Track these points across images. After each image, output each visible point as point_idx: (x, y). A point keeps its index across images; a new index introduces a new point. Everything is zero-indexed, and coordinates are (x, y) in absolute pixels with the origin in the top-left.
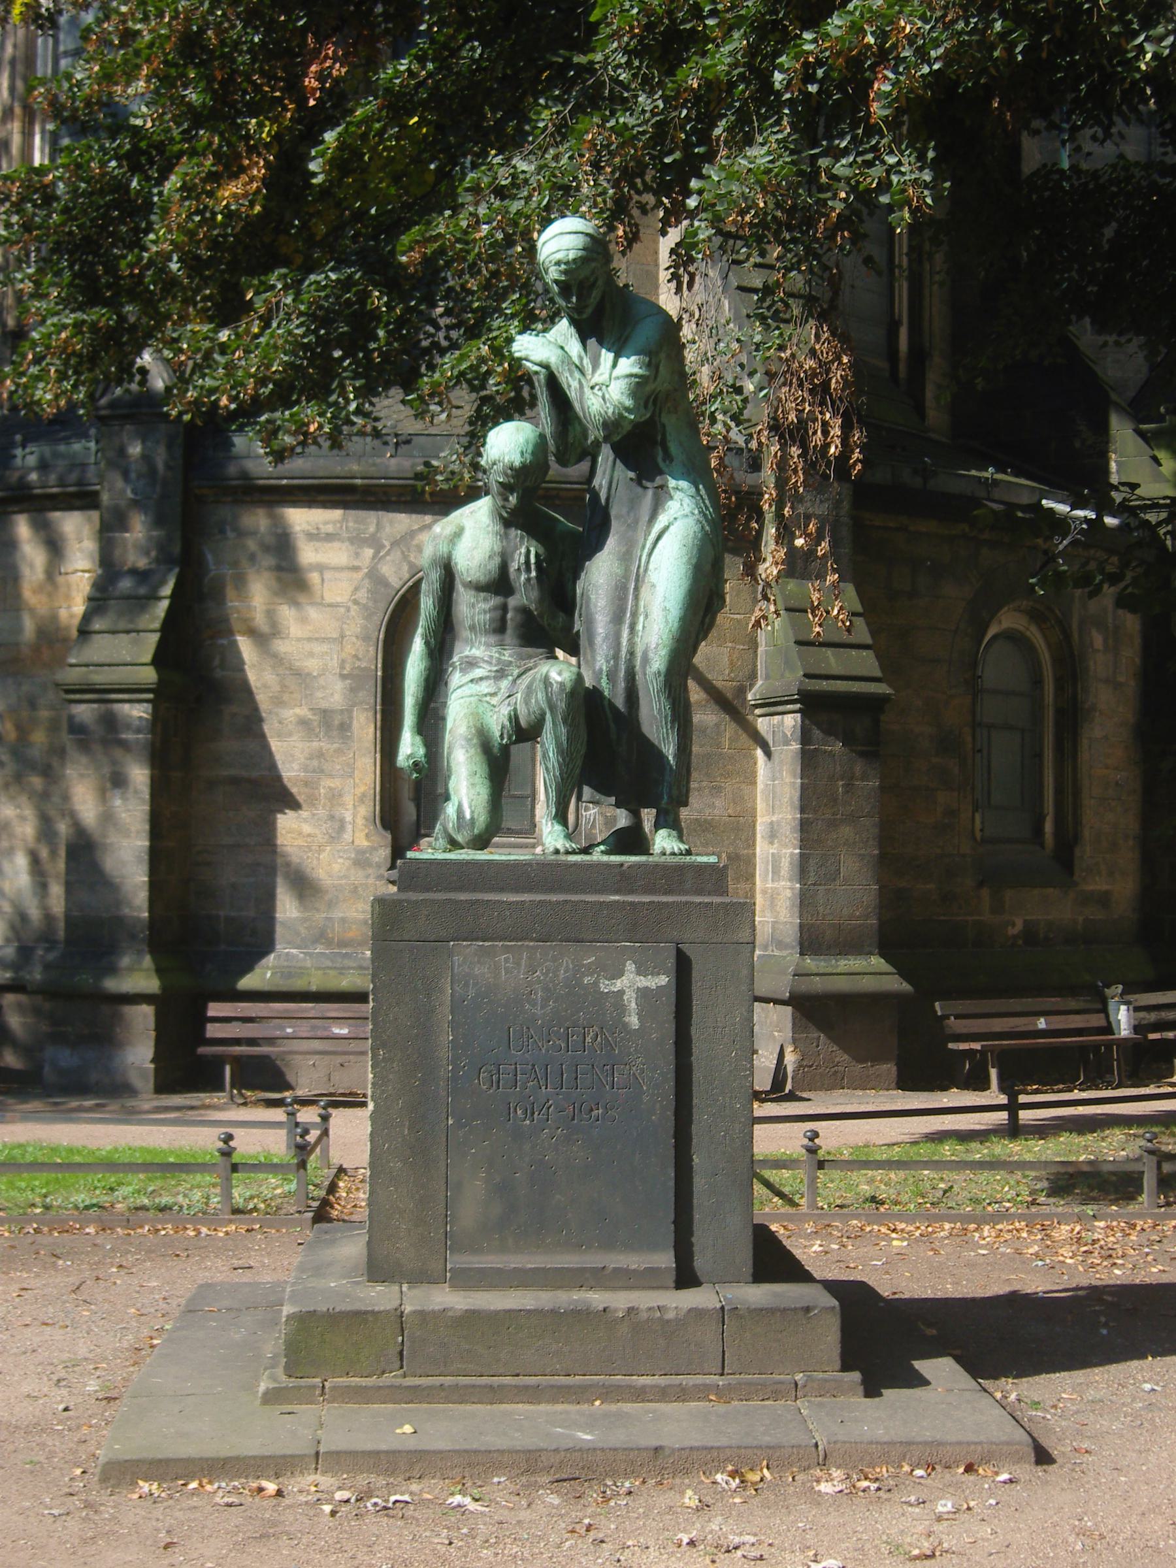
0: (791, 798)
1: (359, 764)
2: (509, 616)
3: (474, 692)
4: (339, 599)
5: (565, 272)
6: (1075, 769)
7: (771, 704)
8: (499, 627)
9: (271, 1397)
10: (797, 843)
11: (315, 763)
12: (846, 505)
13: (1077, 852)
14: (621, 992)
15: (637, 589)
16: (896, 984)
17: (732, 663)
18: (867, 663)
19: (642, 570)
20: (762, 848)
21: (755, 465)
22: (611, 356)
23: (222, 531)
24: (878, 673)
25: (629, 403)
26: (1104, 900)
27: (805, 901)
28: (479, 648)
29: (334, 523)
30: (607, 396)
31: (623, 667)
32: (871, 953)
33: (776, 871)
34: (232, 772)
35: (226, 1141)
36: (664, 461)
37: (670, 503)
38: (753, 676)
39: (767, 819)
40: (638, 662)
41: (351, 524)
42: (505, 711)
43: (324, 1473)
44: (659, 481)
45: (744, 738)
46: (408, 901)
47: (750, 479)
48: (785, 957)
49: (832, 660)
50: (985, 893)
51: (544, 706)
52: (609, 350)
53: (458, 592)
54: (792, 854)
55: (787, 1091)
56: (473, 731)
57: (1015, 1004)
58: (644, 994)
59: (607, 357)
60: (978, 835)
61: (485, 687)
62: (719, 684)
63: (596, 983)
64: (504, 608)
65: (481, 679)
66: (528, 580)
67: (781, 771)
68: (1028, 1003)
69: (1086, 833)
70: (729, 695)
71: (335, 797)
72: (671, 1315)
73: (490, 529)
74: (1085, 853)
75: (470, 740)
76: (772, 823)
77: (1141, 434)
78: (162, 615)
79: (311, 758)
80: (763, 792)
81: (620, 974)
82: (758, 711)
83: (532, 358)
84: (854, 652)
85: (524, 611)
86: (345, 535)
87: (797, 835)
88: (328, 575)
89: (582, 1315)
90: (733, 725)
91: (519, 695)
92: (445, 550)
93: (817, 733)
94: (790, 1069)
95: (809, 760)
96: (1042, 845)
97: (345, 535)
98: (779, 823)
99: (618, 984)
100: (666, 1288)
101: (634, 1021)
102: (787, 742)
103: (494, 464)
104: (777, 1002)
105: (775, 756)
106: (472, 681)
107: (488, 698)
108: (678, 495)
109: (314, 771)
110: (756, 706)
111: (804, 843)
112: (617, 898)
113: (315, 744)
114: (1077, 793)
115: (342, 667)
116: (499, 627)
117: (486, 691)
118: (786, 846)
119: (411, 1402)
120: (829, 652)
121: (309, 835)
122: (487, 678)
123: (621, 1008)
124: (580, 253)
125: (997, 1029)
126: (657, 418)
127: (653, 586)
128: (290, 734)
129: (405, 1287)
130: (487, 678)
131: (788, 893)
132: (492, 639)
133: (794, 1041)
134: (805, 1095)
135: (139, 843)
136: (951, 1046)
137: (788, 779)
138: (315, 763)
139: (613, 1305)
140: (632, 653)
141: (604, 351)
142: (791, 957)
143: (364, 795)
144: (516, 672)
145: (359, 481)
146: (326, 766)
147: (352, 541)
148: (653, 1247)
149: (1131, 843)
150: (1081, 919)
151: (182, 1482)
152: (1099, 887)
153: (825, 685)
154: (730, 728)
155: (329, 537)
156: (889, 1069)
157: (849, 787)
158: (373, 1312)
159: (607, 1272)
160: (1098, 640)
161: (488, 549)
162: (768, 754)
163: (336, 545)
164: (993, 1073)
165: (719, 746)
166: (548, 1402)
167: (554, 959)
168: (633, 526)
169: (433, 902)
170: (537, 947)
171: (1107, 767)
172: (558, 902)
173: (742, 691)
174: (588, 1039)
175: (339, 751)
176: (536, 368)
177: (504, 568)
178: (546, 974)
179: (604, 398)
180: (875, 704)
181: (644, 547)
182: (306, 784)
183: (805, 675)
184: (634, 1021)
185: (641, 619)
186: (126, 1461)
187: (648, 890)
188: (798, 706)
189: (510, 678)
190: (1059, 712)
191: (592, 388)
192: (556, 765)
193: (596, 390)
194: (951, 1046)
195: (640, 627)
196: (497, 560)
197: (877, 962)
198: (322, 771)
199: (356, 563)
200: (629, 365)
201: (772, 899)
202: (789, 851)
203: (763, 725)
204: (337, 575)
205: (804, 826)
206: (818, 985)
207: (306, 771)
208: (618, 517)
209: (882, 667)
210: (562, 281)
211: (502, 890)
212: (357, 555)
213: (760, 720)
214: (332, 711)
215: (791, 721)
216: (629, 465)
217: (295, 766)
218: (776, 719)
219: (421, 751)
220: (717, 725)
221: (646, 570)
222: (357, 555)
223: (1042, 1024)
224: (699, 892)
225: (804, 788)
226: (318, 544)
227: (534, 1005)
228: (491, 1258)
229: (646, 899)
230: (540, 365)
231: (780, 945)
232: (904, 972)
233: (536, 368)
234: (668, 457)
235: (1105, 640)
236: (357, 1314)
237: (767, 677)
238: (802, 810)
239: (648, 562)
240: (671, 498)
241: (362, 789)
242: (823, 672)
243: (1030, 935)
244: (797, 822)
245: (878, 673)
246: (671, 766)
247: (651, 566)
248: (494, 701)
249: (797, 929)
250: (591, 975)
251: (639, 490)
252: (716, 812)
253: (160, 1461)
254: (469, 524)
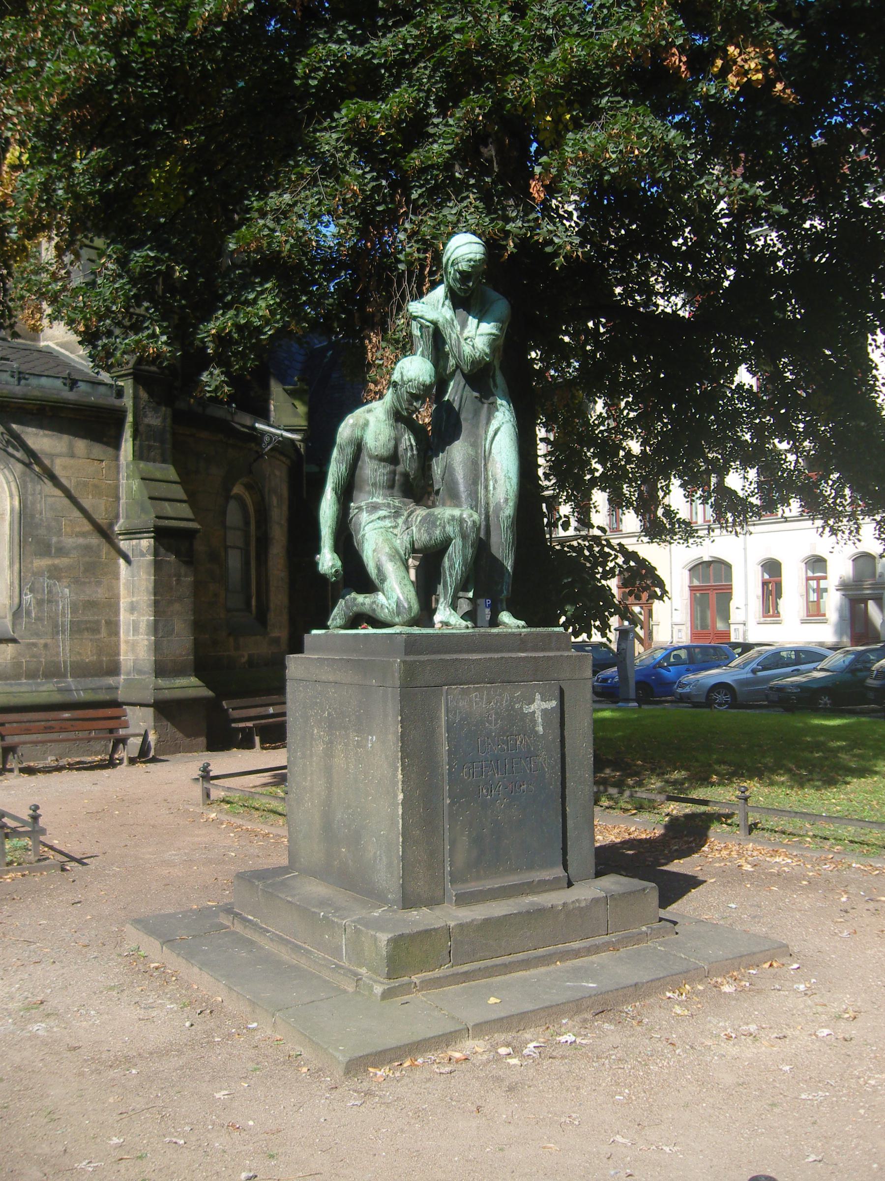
0: (147, 588)
2: (397, 478)
5: (472, 267)
7: (132, 533)
8: (391, 486)
9: (387, 994)
10: (152, 613)
12: (169, 421)
14: (534, 712)
15: (485, 465)
16: (207, 693)
17: (106, 510)
18: (185, 510)
19: (487, 453)
20: (124, 617)
21: (120, 393)
22: (476, 321)
24: (191, 516)
25: (487, 351)
27: (157, 647)
32: (190, 675)
33: (136, 630)
37: (497, 413)
38: (117, 517)
39: (129, 600)
42: (406, 538)
43: (473, 1038)
44: (491, 399)
45: (113, 553)
46: (420, 662)
47: (117, 402)
48: (144, 680)
49: (169, 508)
50: (231, 640)
52: (474, 317)
53: (364, 462)
54: (148, 620)
55: (151, 756)
57: (258, 700)
58: (545, 712)
59: (472, 321)
61: (388, 523)
62: (100, 521)
63: (521, 708)
64: (394, 473)
65: (385, 517)
66: (413, 455)
68: (264, 699)
69: (272, 606)
70: (105, 527)
72: (583, 904)
75: (394, 556)
77: (285, 390)
80: (124, 584)
82: (121, 537)
83: (426, 317)
84: (179, 504)
85: (406, 475)
87: (152, 609)
89: (541, 912)
90: (107, 545)
93: (162, 550)
94: (152, 744)
95: (158, 565)
96: (251, 612)
98: (137, 602)
99: (533, 707)
100: (563, 888)
101: (540, 729)
102: (143, 555)
103: (411, 381)
104: (142, 705)
105: (134, 564)
108: (501, 409)
110: (120, 534)
111: (157, 613)
116: (391, 486)
117: (390, 525)
118: (144, 615)
119: (465, 982)
120: (166, 504)
123: (534, 721)
124: (483, 256)
125: (252, 715)
130: (389, 517)
131: (146, 643)
132: (388, 492)
133: (155, 728)
134: (162, 758)
136: (233, 725)
137: (143, 576)
139: (555, 902)
140: (487, 504)
141: (470, 318)
142: (150, 680)
144: (406, 514)
148: (552, 865)
151: (396, 1064)
153: (166, 523)
154: (105, 548)
156: (202, 740)
157: (178, 581)
158: (434, 929)
159: (535, 883)
162: (128, 561)
164: (257, 739)
165: (99, 557)
166: (533, 967)
167: (500, 695)
168: (476, 425)
169: (433, 661)
170: (491, 687)
172: (498, 659)
173: (111, 525)
174: (518, 743)
176: (428, 324)
177: (396, 447)
178: (496, 704)
179: (473, 346)
180: (189, 534)
181: (486, 439)
183: (157, 517)
184: (540, 729)
185: (491, 483)
186: (360, 1057)
187: (534, 649)
188: (153, 534)
190: (258, 540)
191: (466, 339)
192: (459, 572)
193: (468, 341)
194: (233, 725)
195: (491, 488)
196: (393, 442)
197: (194, 680)
200: (488, 328)
201: (133, 646)
202: (146, 618)
203: (124, 545)
205: (156, 603)
206: (167, 695)
208: (466, 420)
209: (194, 513)
211: (460, 652)
213: (122, 542)
215: (146, 543)
216: (474, 389)
218: (134, 542)
219: (339, 564)
220: (99, 545)
223: (271, 710)
224: (558, 650)
225: (155, 581)
227: (490, 724)
228: (473, 884)
229: (541, 654)
230: (431, 322)
231: (140, 672)
232: (209, 685)
233: (428, 324)
234: (495, 385)
236: (426, 931)
237: (127, 517)
238: (155, 594)
240: (498, 410)
242: (165, 515)
243: (251, 663)
244: (152, 602)
245: (191, 516)
246: (509, 573)
247: (493, 451)
248: (395, 531)
249: (153, 663)
251: (480, 404)
252: (99, 596)
253: (381, 1052)
254: (371, 418)
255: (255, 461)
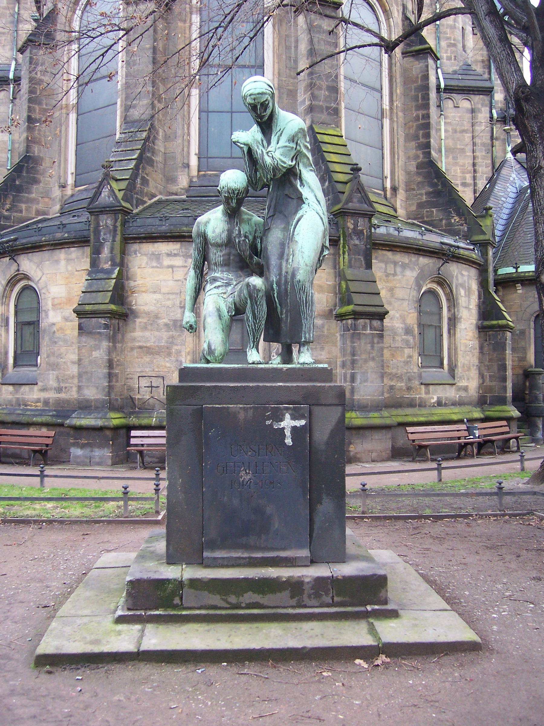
1: (187, 340)
3: (216, 292)
4: (179, 278)
6: (455, 340)
11: (171, 340)
13: (456, 371)
14: (283, 428)
23: (136, 254)
26: (466, 389)
28: (218, 273)
29: (177, 250)
30: (274, 156)
31: (283, 279)
34: (141, 344)
35: (126, 488)
36: (301, 186)
37: (303, 205)
39: (341, 359)
40: (289, 277)
41: (183, 250)
51: (247, 296)
56: (215, 309)
60: (420, 365)
65: (219, 286)
67: (346, 341)
69: (459, 364)
71: (179, 352)
73: (223, 219)
74: (459, 371)
76: (343, 361)
78: (113, 285)
79: (169, 338)
81: (282, 420)
86: (181, 254)
88: (175, 269)
91: (236, 293)
92: (203, 229)
97: (181, 254)
98: (346, 361)
106: (215, 287)
107: (222, 295)
109: (171, 343)
112: (281, 384)
113: (171, 333)
114: (456, 349)
115: (180, 304)
117: (221, 292)
118: (349, 369)
121: (169, 367)
122: (222, 286)
126: (297, 167)
127: (297, 242)
128: (161, 329)
129: (184, 566)
130: (222, 286)
135: (105, 371)
138: (171, 340)
143: (189, 352)
144: (235, 283)
145: (187, 234)
146: (175, 341)
147: (183, 256)
149: (475, 367)
150: (458, 396)
152: (463, 384)
155: (175, 255)
160: (462, 292)
161: (222, 228)
163: (178, 258)
165: (323, 332)
171: (466, 340)
175: (179, 336)
182: (167, 348)
185: (291, 257)
189: (232, 286)
190: (449, 319)
198: (173, 343)
199: (186, 265)
204: (179, 269)
207: (167, 343)
210: (252, 104)
212: (186, 261)
214: (177, 320)
217: (164, 341)
221: (293, 234)
222: (186, 261)
226: (171, 258)
230: (244, 144)
235: (465, 293)
239: (294, 231)
241: (188, 350)
247: (295, 233)
250: (269, 420)
255: (443, 265)
